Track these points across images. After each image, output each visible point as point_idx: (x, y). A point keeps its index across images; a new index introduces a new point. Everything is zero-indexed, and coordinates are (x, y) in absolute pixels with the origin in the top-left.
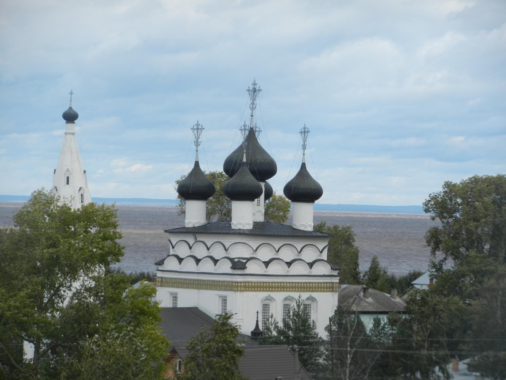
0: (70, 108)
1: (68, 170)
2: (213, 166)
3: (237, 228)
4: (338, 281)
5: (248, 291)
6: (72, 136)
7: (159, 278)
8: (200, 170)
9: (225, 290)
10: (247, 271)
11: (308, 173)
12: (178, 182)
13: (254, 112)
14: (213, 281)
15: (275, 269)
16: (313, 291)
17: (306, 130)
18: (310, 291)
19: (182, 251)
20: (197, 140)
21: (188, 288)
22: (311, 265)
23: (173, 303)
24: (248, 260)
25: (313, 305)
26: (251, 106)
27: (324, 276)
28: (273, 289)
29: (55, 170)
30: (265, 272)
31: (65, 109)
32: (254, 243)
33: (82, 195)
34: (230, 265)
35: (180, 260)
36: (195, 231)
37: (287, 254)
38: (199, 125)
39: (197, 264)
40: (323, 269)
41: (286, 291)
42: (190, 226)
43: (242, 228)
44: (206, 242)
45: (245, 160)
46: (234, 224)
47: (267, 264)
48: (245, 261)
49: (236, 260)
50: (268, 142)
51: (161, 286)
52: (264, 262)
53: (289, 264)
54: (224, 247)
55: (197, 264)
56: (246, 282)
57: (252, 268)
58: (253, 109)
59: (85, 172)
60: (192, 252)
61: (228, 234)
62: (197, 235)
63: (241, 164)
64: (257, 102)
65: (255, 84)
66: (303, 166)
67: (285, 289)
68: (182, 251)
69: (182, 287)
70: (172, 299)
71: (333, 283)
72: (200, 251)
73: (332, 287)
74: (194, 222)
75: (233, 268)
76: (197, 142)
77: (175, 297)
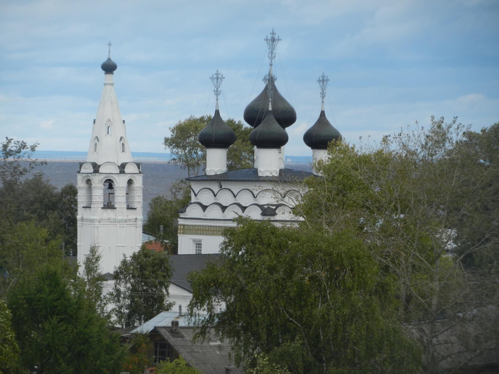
0: (109, 59)
1: (109, 120)
2: (234, 113)
3: (265, 175)
6: (111, 86)
7: (181, 225)
8: (220, 119)
9: (200, 234)
11: (327, 121)
13: (273, 61)
17: (325, 78)
19: (206, 198)
20: (217, 89)
21: (213, 235)
23: (196, 250)
24: (278, 206)
26: (270, 55)
29: (95, 121)
31: (104, 60)
32: (281, 189)
33: (123, 144)
34: (260, 212)
35: (204, 208)
36: (219, 179)
38: (219, 74)
39: (223, 211)
42: (212, 174)
43: (269, 175)
45: (270, 109)
46: (261, 171)
48: (274, 207)
49: (266, 207)
51: (183, 233)
54: (213, 192)
55: (223, 211)
59: (124, 122)
60: (217, 200)
63: (268, 112)
65: (273, 33)
66: (323, 113)
68: (206, 198)
69: (206, 234)
70: (195, 245)
72: (226, 198)
74: (216, 170)
75: (263, 214)
76: (217, 91)
77: (199, 245)
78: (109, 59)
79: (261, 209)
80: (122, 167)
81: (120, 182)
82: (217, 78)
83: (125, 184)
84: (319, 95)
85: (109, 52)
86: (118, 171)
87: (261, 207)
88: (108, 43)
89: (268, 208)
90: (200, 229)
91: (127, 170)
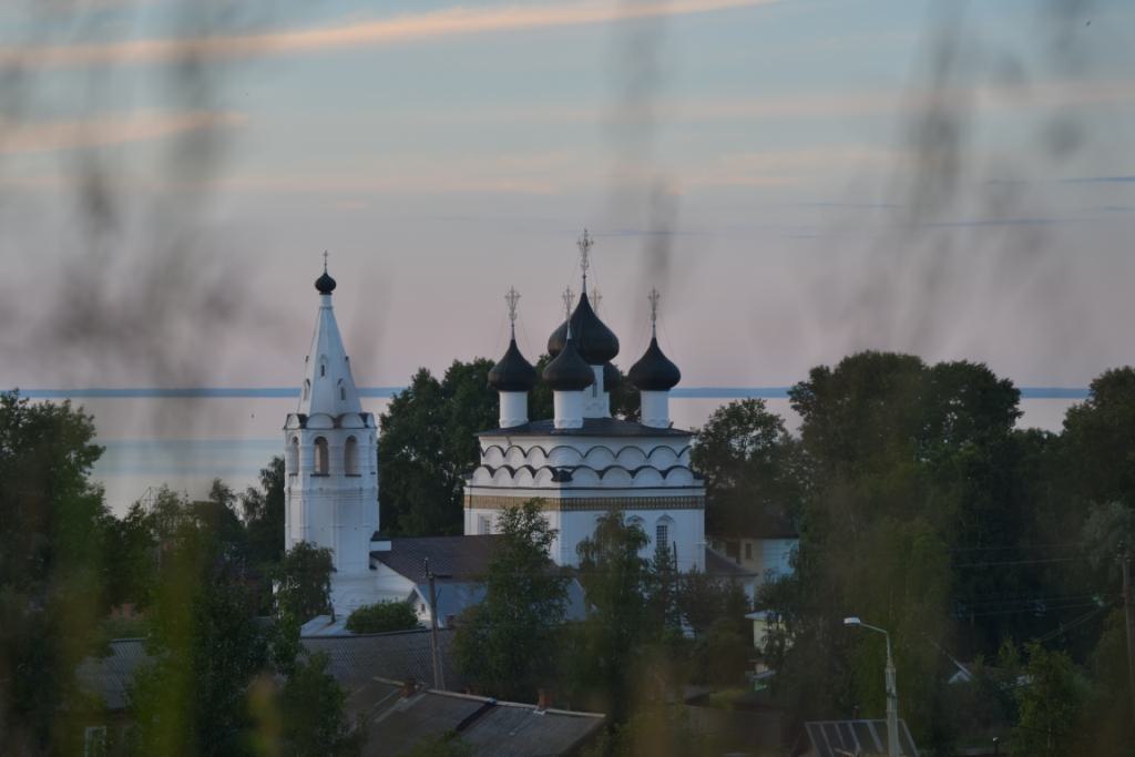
0: (326, 275)
4: (704, 494)
10: (574, 484)
14: (498, 497)
16: (668, 508)
18: (663, 509)
19: (495, 459)
22: (664, 474)
24: (575, 468)
27: (684, 487)
31: (320, 275)
32: (583, 446)
34: (551, 475)
37: (631, 460)
40: (680, 478)
48: (570, 471)
49: (559, 470)
52: (661, 472)
53: (633, 473)
57: (580, 479)
58: (585, 267)
61: (550, 435)
62: (512, 438)
64: (589, 258)
73: (696, 502)
78: (326, 275)
81: (334, 440)
82: (513, 297)
84: (649, 318)
86: (331, 425)
87: (553, 470)
89: (562, 471)
90: (660, 503)
91: (345, 424)
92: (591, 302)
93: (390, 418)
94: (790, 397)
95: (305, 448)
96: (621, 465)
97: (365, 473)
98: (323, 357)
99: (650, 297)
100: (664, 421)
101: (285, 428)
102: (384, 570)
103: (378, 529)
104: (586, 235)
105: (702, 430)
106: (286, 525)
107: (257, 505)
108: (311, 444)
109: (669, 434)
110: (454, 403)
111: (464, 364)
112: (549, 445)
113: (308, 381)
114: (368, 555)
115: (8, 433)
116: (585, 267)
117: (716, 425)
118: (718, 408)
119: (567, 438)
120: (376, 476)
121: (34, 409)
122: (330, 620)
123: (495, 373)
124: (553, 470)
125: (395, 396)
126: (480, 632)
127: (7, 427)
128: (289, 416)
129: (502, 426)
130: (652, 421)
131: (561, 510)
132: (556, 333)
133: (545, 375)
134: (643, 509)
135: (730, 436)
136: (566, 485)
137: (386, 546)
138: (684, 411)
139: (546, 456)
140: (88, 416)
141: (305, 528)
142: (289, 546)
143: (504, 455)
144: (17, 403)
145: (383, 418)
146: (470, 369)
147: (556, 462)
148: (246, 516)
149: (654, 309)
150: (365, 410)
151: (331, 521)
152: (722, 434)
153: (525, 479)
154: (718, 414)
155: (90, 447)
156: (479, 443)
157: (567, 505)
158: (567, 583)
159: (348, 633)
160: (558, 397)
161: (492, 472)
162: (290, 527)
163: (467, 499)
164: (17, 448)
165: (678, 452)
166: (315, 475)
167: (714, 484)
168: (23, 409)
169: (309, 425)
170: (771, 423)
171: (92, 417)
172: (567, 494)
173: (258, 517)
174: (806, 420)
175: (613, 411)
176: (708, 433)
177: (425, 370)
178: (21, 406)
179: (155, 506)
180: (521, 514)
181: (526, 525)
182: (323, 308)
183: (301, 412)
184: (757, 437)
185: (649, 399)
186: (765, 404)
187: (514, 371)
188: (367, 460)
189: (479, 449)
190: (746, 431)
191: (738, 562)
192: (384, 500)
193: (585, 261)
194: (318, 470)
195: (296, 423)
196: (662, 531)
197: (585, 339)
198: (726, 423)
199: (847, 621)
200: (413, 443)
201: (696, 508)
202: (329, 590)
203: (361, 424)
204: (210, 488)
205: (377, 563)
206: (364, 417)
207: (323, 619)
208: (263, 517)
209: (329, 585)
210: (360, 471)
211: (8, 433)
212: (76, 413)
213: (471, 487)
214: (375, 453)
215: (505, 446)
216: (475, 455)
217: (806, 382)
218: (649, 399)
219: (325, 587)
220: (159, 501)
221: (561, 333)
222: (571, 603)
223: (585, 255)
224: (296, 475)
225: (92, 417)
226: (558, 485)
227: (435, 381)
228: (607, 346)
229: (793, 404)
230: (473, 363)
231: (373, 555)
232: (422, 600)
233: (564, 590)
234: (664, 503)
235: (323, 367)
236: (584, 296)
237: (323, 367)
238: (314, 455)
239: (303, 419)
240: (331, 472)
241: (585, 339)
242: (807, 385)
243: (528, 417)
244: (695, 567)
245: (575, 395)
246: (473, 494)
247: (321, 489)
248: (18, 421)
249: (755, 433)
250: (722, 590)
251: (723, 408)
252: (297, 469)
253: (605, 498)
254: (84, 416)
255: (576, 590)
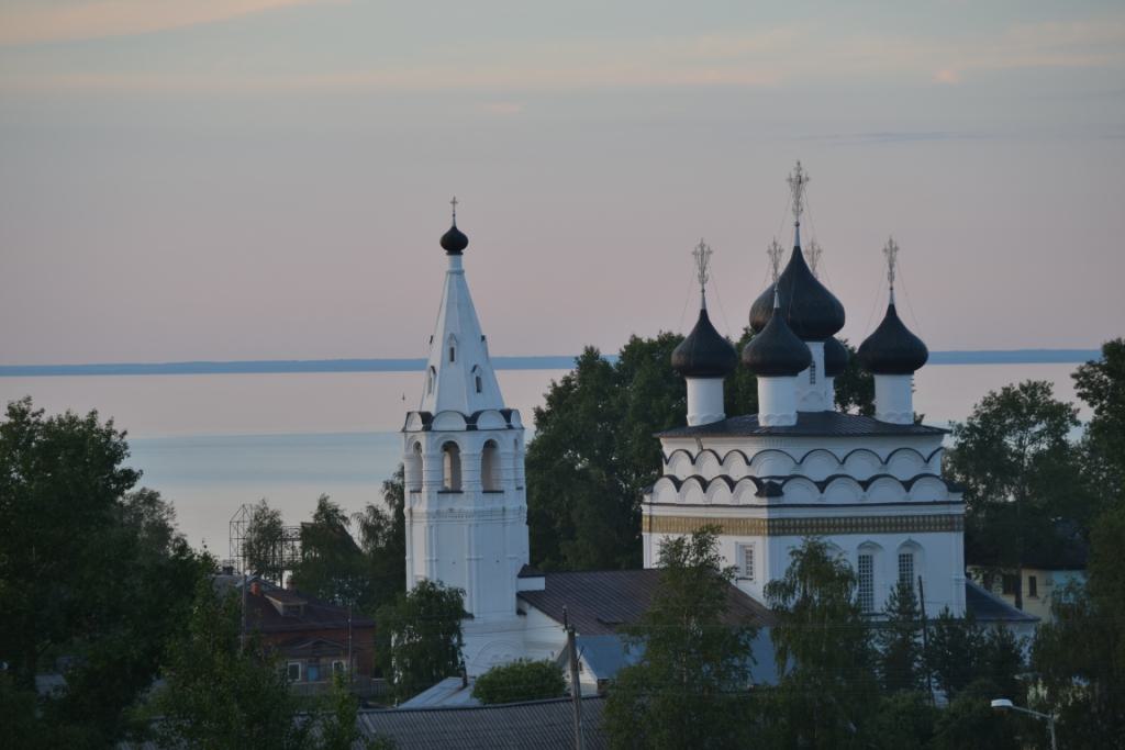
0: (454, 229)
5: (789, 534)
9: (749, 534)
12: (1119, 340)
14: (687, 518)
15: (838, 493)
18: (907, 531)
19: (682, 468)
21: (930, 531)
24: (787, 479)
25: (917, 557)
27: (935, 503)
28: (837, 530)
30: (819, 499)
31: (447, 228)
32: (797, 449)
33: (478, 380)
34: (753, 488)
40: (931, 491)
41: (863, 532)
44: (920, 450)
47: (822, 486)
48: (780, 482)
49: (765, 481)
50: (830, 276)
52: (903, 483)
54: (690, 456)
56: (783, 519)
61: (752, 435)
64: (803, 199)
66: (892, 310)
67: (860, 529)
71: (952, 516)
78: (454, 229)
79: (758, 486)
80: (472, 422)
81: (470, 447)
83: (479, 450)
84: (696, 280)
85: (454, 215)
86: (464, 425)
87: (757, 481)
88: (452, 199)
89: (770, 483)
91: (480, 424)
92: (806, 258)
93: (549, 413)
94: (1075, 382)
95: (432, 457)
96: (892, 474)
97: (510, 488)
98: (452, 337)
99: (885, 250)
100: (907, 415)
101: (404, 430)
102: (537, 617)
103: (527, 563)
104: (799, 169)
105: (965, 425)
106: (407, 558)
107: (379, 527)
108: (438, 451)
109: (917, 431)
110: (632, 391)
111: (645, 340)
112: (751, 449)
113: (433, 368)
114: (514, 596)
115: (17, 454)
116: (798, 211)
117: (984, 417)
118: (987, 395)
119: (776, 438)
120: (524, 493)
121: (51, 422)
122: (461, 684)
123: (680, 353)
124: (757, 481)
125: (554, 384)
126: (638, 701)
127: (16, 446)
128: (409, 414)
129: (690, 424)
130: (890, 415)
131: (769, 534)
132: (759, 302)
133: (745, 357)
134: (879, 532)
135: (1005, 431)
136: (775, 501)
137: (538, 584)
138: (943, 398)
139: (748, 463)
140: (120, 432)
141: (431, 561)
142: (411, 585)
143: (693, 462)
144: (29, 416)
145: (539, 414)
146: (651, 348)
147: (763, 470)
148: (365, 543)
149: (891, 266)
150: (508, 406)
151: (467, 549)
152: (993, 430)
153: (721, 493)
154: (987, 403)
155: (123, 471)
156: (661, 447)
157: (777, 528)
158: (750, 637)
159: (476, 702)
160: (763, 384)
161: (678, 484)
162: (412, 560)
163: (645, 520)
164: (29, 475)
165: (926, 456)
166: (445, 492)
167: (984, 497)
168: (37, 423)
169: (435, 426)
170: (1059, 416)
171: (125, 433)
172: (777, 514)
173: (382, 544)
174: (1098, 412)
175: (842, 399)
176: (972, 428)
177: (592, 349)
178: (33, 419)
179: (249, 530)
180: (688, 547)
181: (696, 560)
182: (452, 273)
183: (424, 410)
184: (1041, 434)
185: (884, 385)
186: (1052, 389)
187: (706, 351)
188: (512, 470)
189: (663, 455)
190: (1025, 425)
191: (1019, 604)
192: (537, 520)
193: (798, 203)
194: (448, 485)
195: (418, 424)
196: (905, 562)
197: (800, 308)
198: (997, 414)
199: (995, 703)
200: (581, 444)
201: (952, 530)
202: (460, 644)
203: (503, 424)
204: (314, 508)
205: (526, 606)
206: (507, 414)
207: (452, 682)
208: (388, 543)
209: (460, 639)
210: (503, 486)
211: (17, 454)
212: (104, 427)
213: (651, 504)
214: (522, 465)
215: (694, 451)
216: (658, 460)
217: (1097, 361)
218: (884, 385)
219: (455, 640)
220: (255, 524)
221: (767, 299)
222: (756, 663)
223: (798, 196)
224: (419, 491)
225: (125, 433)
226: (765, 501)
227: (606, 364)
228: (829, 315)
229: (1079, 391)
230: (656, 339)
231: (521, 596)
232: (982, 589)
233: (747, 646)
234: (913, 524)
235: (452, 350)
236: (797, 250)
237: (452, 350)
238: (443, 464)
239: (427, 418)
240: (464, 488)
241: (800, 308)
242: (1099, 365)
243: (726, 411)
244: (947, 610)
245: (785, 383)
246: (654, 513)
247: (451, 510)
248: (29, 441)
249: (1038, 428)
250: (987, 642)
251: (994, 395)
252: (420, 484)
253: (828, 519)
254: (115, 432)
255: (763, 645)
